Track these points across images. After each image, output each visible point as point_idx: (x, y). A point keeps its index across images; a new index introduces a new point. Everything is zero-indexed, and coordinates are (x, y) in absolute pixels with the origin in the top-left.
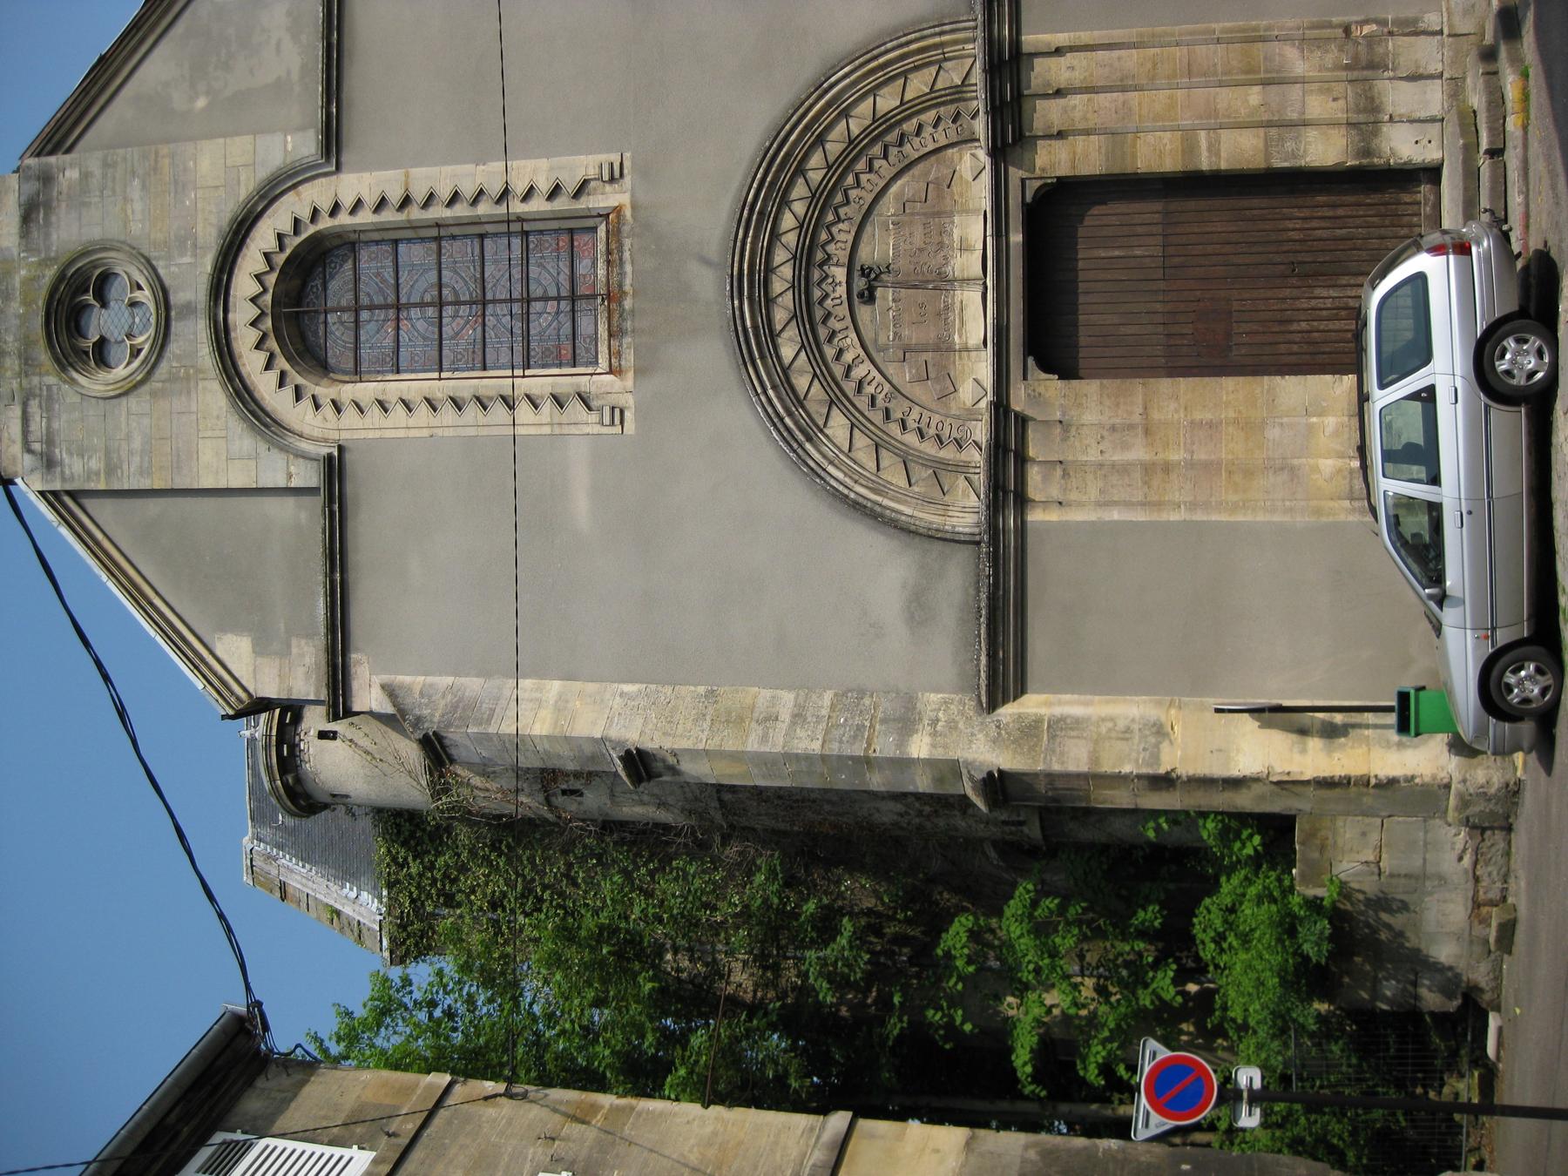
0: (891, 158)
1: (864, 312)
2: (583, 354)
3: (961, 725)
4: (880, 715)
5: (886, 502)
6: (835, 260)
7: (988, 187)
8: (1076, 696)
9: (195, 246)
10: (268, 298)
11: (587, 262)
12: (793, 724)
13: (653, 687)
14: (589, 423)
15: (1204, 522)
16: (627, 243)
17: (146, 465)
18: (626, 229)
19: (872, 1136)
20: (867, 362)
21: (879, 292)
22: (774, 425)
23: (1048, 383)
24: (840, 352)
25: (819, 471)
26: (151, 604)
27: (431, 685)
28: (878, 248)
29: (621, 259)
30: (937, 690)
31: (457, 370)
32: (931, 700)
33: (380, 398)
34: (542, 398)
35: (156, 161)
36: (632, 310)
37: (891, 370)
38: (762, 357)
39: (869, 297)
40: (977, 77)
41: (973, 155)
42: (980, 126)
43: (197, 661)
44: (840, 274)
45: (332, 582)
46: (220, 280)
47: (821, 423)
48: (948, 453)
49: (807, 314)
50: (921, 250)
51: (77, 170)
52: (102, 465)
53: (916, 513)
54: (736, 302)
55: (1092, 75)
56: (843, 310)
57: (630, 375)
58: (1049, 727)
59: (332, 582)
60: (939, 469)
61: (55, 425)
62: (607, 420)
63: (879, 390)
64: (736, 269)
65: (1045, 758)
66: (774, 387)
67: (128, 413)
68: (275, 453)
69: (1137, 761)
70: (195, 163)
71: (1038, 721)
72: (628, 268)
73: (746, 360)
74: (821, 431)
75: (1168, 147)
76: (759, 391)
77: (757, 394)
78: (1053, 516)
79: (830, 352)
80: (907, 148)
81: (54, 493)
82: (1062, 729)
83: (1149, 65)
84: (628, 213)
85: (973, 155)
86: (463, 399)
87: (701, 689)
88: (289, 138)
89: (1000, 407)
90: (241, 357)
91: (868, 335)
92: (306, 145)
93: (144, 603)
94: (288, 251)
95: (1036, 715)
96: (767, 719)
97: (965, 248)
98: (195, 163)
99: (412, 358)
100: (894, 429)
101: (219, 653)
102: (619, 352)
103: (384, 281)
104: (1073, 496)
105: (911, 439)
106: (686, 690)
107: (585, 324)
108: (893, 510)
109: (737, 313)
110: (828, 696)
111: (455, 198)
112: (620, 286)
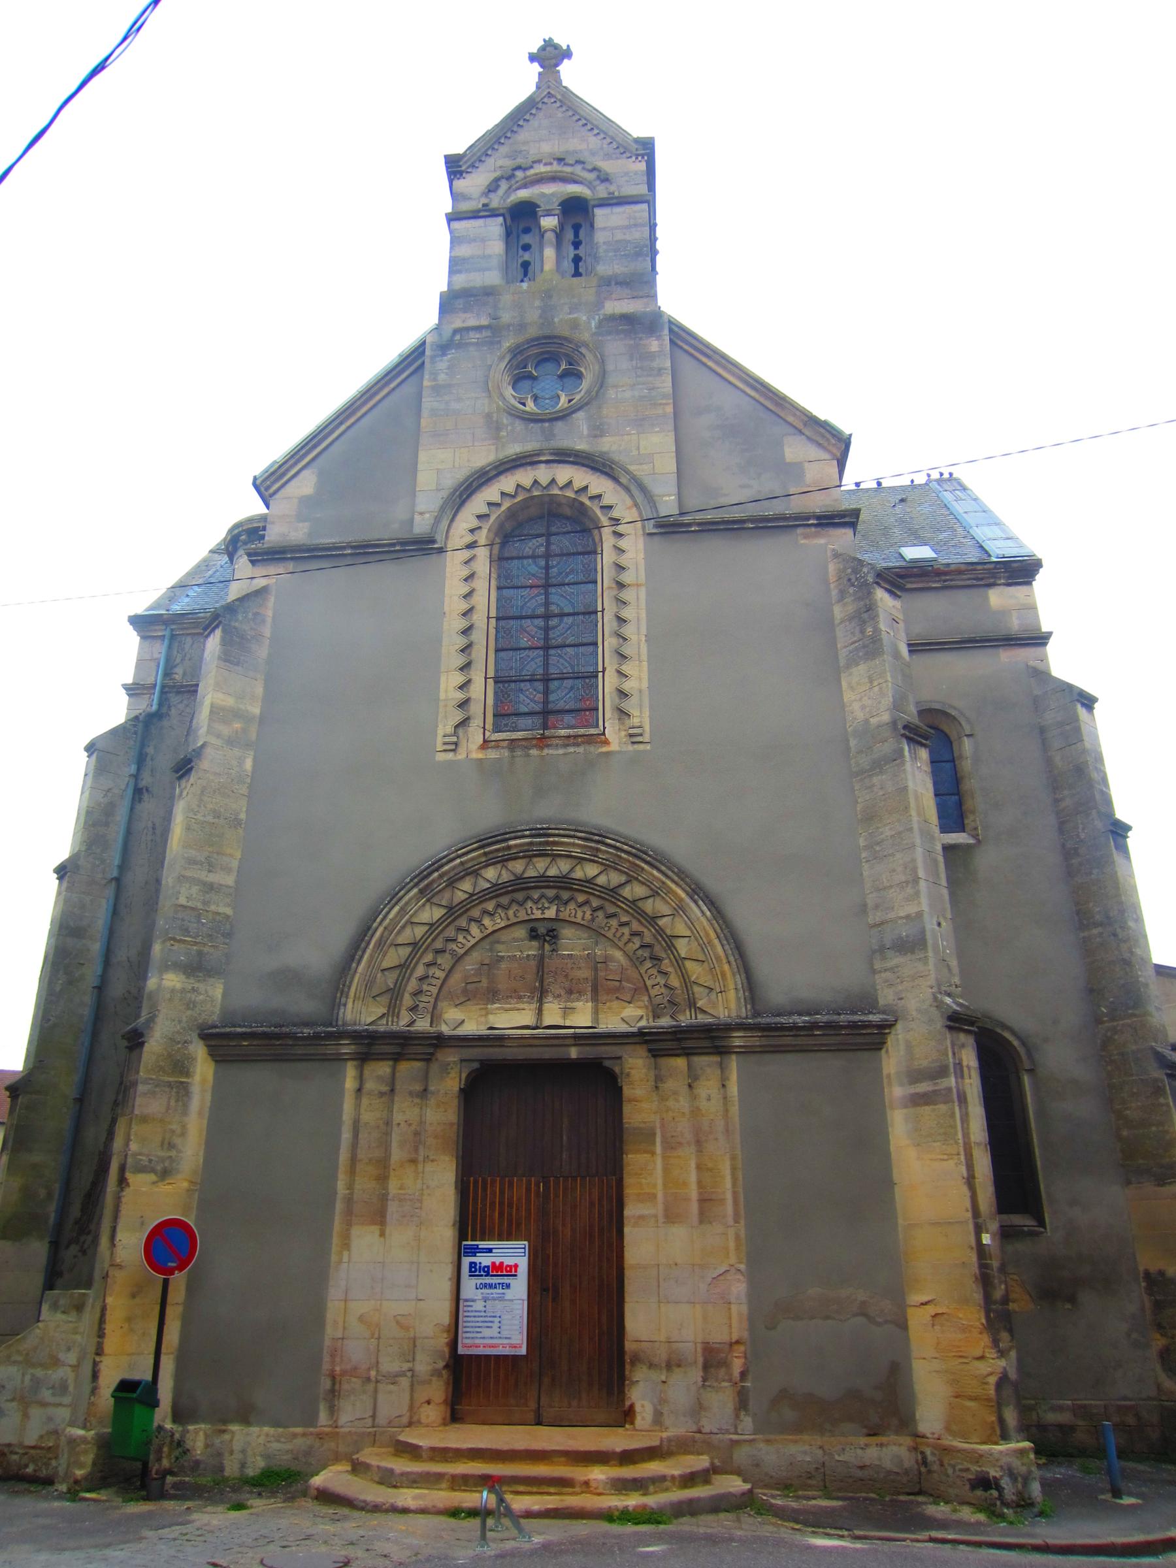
0: (640, 952)
1: (521, 932)
2: (504, 722)
3: (189, 1013)
4: (206, 950)
5: (368, 952)
6: (562, 909)
7: (614, 1030)
8: (209, 1104)
9: (596, 436)
11: (573, 722)
12: (204, 884)
13: (249, 780)
14: (445, 727)
15: (334, 1207)
16: (581, 749)
18: (592, 748)
20: (481, 936)
21: (535, 943)
22: (433, 864)
23: (458, 1079)
24: (491, 915)
25: (395, 900)
26: (341, 423)
27: (264, 621)
28: (573, 943)
29: (568, 745)
30: (224, 995)
31: (497, 632)
32: (216, 990)
33: (476, 576)
34: (468, 692)
35: (661, 404)
36: (528, 755)
37: (476, 955)
38: (485, 854)
39: (534, 935)
40: (702, 1019)
41: (642, 1017)
42: (665, 1022)
43: (297, 457)
44: (551, 913)
45: (344, 548)
46: (569, 455)
47: (435, 900)
48: (407, 1000)
49: (519, 887)
50: (566, 976)
51: (657, 349)
52: (440, 382)
53: (357, 975)
54: (528, 833)
55: (703, 1116)
56: (522, 916)
57: (480, 756)
58: (182, 1083)
59: (344, 548)
60: (394, 995)
61: (472, 349)
63: (459, 945)
64: (553, 831)
65: (152, 1079)
66: (462, 863)
67: (477, 398)
68: (439, 503)
69: (140, 1154)
70: (658, 432)
71: (188, 1074)
72: (561, 751)
73: (483, 842)
74: (428, 900)
75: (644, 1181)
76: (459, 852)
77: (457, 851)
78: (350, 1084)
79: (490, 906)
80: (648, 964)
81: (424, 352)
82: (178, 1093)
83: (710, 1165)
84: (604, 749)
85: (642, 1017)
87: (243, 816)
88: (673, 498)
89: (440, 1041)
91: (505, 936)
94: (588, 503)
95: (194, 1072)
96: (210, 864)
97: (566, 1011)
98: (656, 432)
100: (429, 958)
102: (498, 747)
103: (567, 575)
104: (365, 1101)
105: (420, 971)
106: (243, 803)
107: (528, 721)
108: (362, 957)
109: (519, 834)
110: (229, 911)
111: (621, 621)
112: (548, 746)
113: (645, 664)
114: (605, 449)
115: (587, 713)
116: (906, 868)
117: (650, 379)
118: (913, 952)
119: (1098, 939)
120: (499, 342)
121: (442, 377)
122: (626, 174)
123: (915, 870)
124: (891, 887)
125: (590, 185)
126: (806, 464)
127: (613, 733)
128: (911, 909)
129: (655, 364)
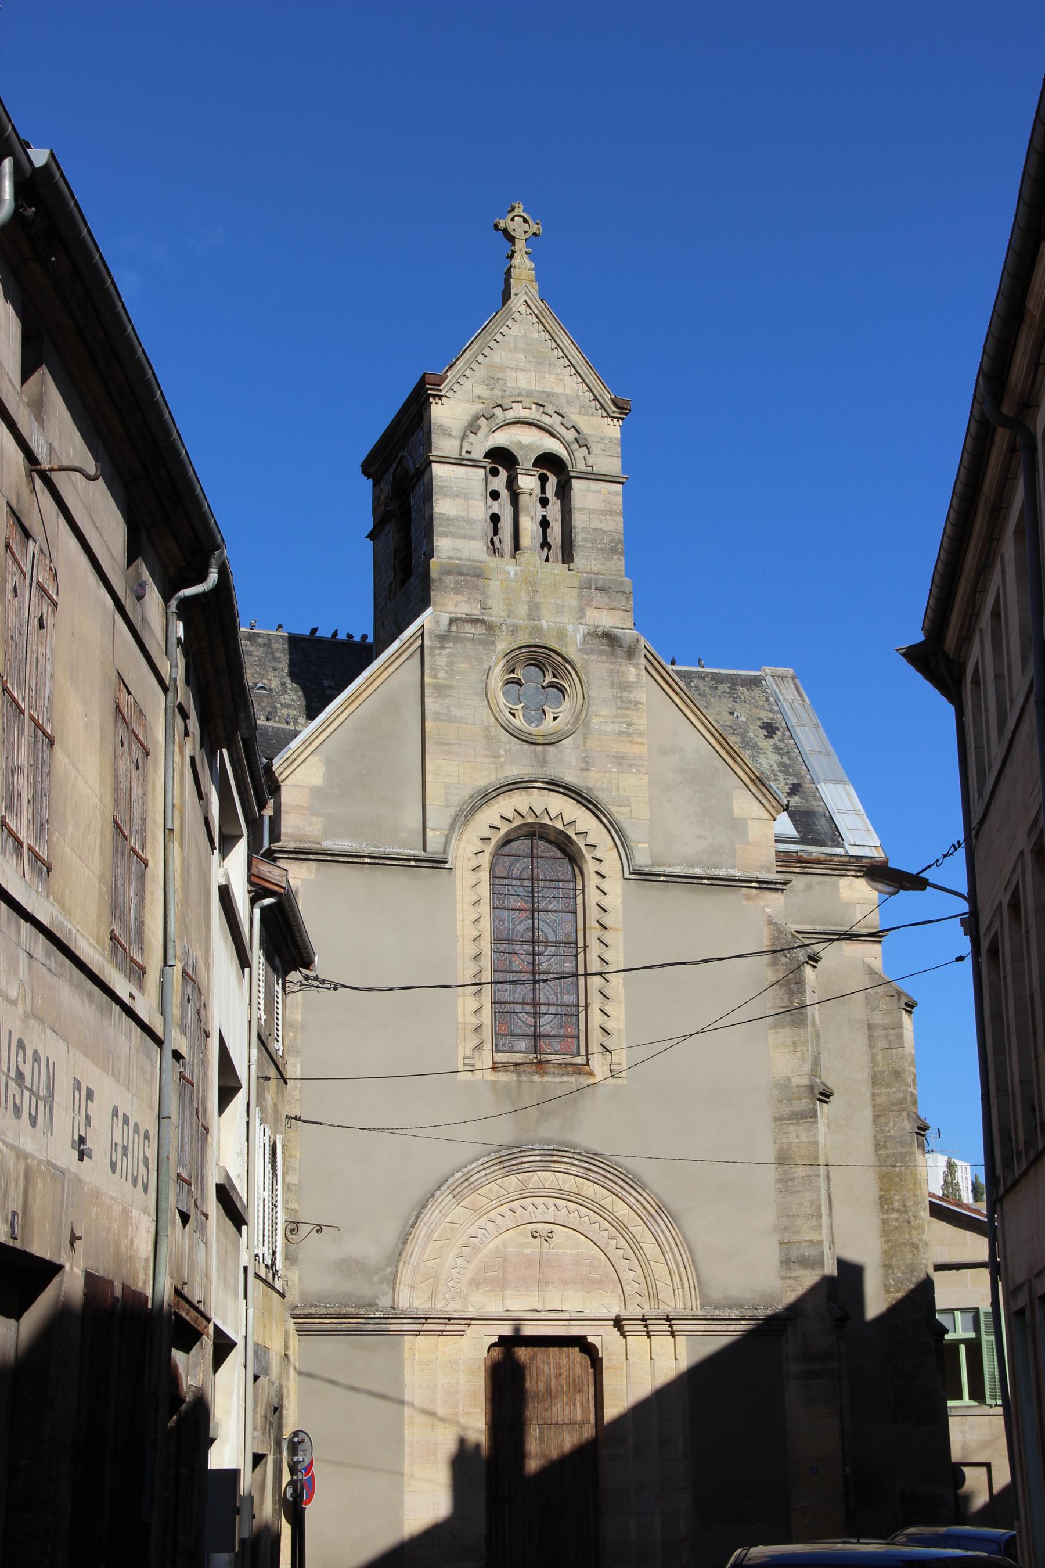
10: (547, 821)
17: (442, 717)
19: (964, 1447)
30: (300, 1279)
62: (467, 1061)
72: (558, 1080)
86: (480, 960)
88: (646, 845)
90: (510, 797)
92: (642, 859)
93: (347, 703)
94: (574, 837)
99: (501, 920)
101: (311, 758)
113: (623, 1005)
114: (590, 785)
115: (569, 1040)
116: (812, 1204)
117: (629, 712)
118: (813, 1269)
119: (894, 1223)
120: (494, 643)
121: (442, 674)
122: (602, 438)
123: (819, 1207)
124: (799, 1216)
125: (567, 446)
126: (750, 822)
127: (599, 1065)
128: (814, 1236)
129: (632, 696)
